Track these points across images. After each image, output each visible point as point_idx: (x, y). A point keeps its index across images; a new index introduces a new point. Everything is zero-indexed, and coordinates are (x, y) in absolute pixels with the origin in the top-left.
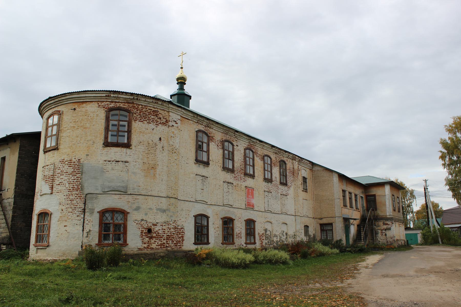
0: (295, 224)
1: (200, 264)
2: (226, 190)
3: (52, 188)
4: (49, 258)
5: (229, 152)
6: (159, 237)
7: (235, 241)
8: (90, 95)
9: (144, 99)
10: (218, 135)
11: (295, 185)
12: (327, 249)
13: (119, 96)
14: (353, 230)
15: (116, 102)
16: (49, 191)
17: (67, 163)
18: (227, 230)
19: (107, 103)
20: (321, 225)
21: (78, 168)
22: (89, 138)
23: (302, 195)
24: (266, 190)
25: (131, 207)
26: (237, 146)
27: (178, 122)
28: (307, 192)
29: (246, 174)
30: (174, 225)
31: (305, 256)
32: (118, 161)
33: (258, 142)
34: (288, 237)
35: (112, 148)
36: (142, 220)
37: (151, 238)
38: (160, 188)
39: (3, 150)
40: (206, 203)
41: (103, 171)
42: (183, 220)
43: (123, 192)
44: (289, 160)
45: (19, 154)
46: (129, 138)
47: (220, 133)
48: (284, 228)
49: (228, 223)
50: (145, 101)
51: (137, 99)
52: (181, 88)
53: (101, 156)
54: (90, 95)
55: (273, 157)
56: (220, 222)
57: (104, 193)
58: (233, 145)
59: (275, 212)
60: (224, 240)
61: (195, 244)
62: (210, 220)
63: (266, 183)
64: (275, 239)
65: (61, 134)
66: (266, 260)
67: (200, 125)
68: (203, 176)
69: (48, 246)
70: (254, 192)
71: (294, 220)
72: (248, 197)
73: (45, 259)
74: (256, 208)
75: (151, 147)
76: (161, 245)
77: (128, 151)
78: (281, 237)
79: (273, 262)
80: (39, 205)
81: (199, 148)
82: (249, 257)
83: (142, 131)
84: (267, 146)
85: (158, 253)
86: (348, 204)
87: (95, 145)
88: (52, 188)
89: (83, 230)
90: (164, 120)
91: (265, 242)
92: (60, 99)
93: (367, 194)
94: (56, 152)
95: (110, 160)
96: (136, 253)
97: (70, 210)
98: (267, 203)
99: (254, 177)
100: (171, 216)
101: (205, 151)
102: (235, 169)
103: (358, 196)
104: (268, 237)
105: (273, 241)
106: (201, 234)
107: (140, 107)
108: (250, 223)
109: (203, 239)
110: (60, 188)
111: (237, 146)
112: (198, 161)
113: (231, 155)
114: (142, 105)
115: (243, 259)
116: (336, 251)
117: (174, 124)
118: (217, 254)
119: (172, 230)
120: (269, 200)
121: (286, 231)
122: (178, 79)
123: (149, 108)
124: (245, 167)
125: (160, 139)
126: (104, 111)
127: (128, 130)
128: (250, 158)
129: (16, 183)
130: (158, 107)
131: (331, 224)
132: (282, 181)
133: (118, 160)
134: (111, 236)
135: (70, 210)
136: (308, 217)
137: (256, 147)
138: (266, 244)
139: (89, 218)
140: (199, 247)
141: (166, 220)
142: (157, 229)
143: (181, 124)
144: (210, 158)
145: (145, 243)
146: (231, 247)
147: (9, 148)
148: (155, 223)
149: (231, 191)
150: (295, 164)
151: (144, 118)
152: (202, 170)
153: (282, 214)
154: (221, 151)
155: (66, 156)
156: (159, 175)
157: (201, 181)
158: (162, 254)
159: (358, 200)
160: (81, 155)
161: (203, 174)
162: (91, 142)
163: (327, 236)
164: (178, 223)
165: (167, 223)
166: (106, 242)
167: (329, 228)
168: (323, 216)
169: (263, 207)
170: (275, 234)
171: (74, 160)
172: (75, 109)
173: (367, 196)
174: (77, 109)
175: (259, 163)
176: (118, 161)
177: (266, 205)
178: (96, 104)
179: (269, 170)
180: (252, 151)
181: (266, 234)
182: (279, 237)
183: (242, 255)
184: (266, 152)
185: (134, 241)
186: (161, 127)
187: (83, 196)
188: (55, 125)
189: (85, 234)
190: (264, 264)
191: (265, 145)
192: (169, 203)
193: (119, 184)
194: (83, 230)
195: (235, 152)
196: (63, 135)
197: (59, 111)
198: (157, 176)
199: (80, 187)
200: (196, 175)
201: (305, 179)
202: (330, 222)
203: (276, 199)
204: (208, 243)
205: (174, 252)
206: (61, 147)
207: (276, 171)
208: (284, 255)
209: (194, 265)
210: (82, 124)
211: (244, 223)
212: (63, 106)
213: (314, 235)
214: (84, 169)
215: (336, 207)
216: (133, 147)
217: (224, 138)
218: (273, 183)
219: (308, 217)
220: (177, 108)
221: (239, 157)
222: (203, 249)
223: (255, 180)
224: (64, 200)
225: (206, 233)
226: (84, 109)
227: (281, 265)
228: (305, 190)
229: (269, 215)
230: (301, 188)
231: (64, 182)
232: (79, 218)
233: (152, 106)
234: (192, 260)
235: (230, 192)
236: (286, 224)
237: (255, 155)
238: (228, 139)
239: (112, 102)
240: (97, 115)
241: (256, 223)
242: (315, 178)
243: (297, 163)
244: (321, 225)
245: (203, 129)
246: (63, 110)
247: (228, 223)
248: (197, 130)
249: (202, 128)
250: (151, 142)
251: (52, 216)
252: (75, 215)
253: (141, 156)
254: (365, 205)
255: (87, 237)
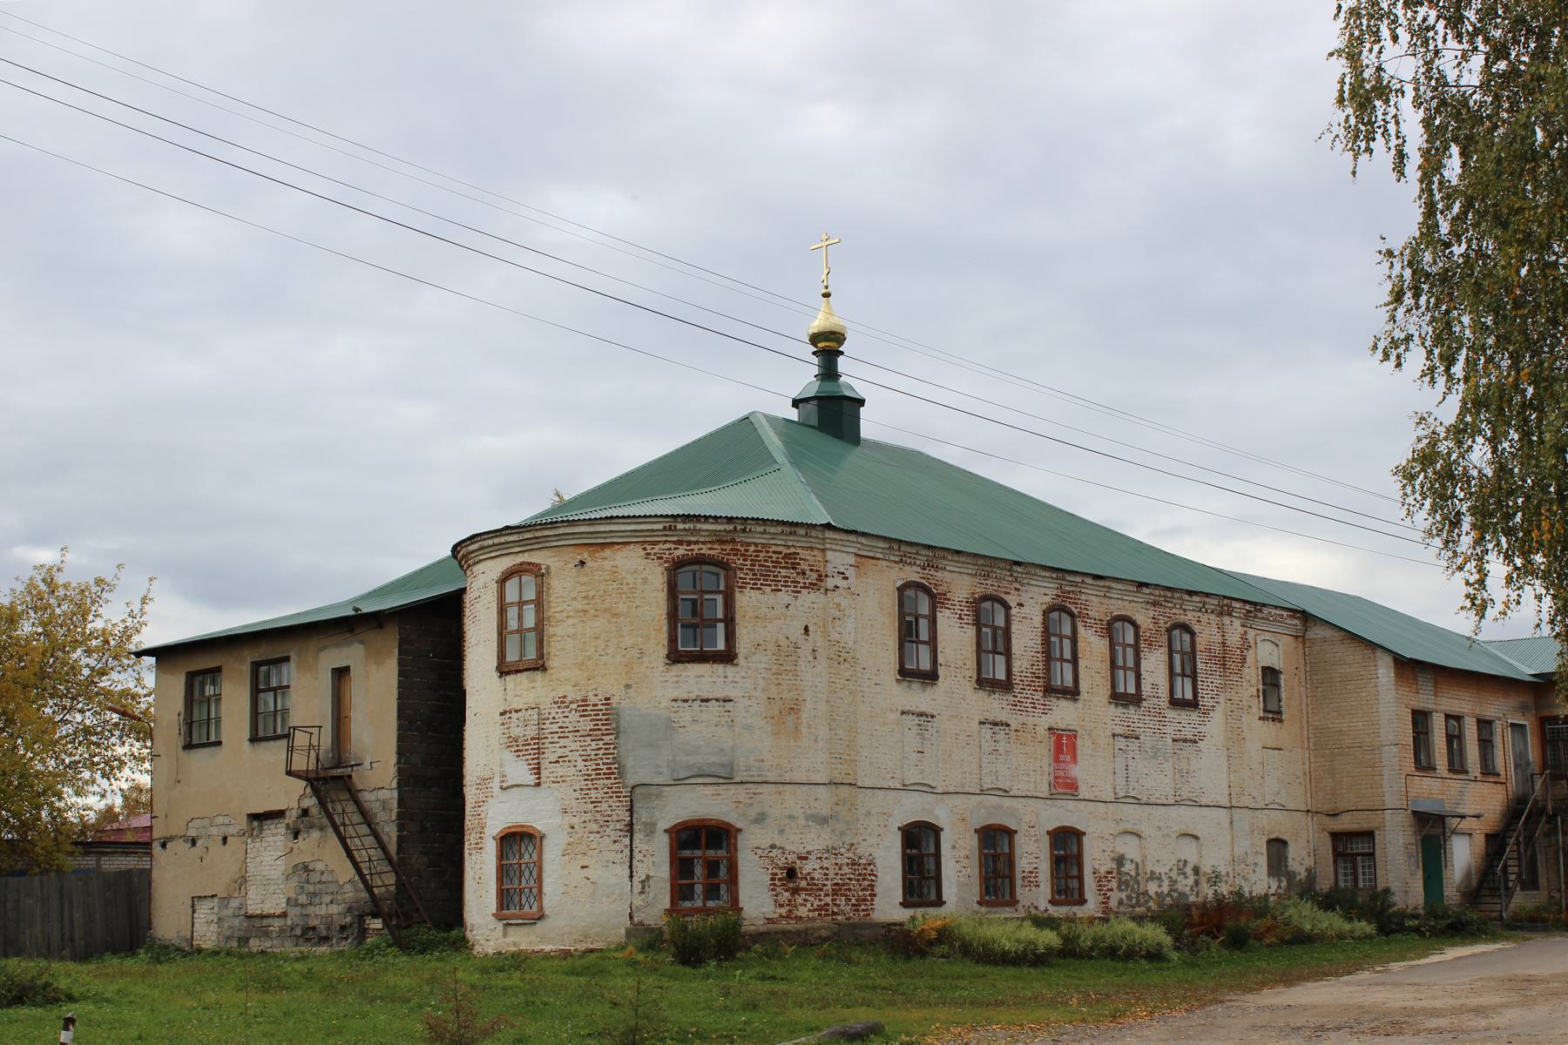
0: (1229, 838)
1: (922, 954)
2: (987, 747)
3: (538, 770)
4: (548, 948)
5: (995, 629)
6: (814, 888)
7: (1019, 897)
8: (623, 528)
9: (761, 529)
10: (960, 585)
11: (1230, 711)
12: (1331, 922)
13: (699, 526)
14: (1462, 855)
15: (689, 543)
16: (532, 779)
17: (574, 706)
18: (995, 862)
19: (668, 546)
20: (1335, 836)
21: (605, 720)
22: (629, 641)
23: (1259, 732)
24: (1119, 730)
25: (744, 815)
26: (1021, 605)
27: (850, 573)
28: (1281, 721)
29: (1049, 690)
30: (851, 855)
31: (1238, 941)
32: (707, 700)
33: (1089, 581)
34: (1203, 880)
35: (689, 666)
36: (773, 846)
37: (796, 891)
38: (813, 761)
39: (336, 645)
40: (930, 789)
41: (670, 726)
42: (871, 840)
43: (724, 777)
44: (1204, 618)
45: (400, 663)
46: (730, 637)
47: (967, 578)
48: (1188, 851)
49: (995, 843)
50: (764, 532)
51: (744, 531)
52: (829, 372)
53: (660, 689)
54: (623, 528)
55: (1143, 618)
56: (974, 841)
57: (678, 782)
58: (1007, 607)
59: (1152, 800)
60: (987, 893)
61: (905, 904)
62: (943, 836)
63: (1120, 709)
64: (1152, 888)
65: (549, 630)
66: (1101, 950)
67: (907, 568)
68: (921, 714)
69: (541, 918)
70: (1079, 742)
71: (1227, 825)
72: (1057, 760)
73: (537, 948)
74: (1084, 792)
75: (786, 655)
76: (820, 908)
77: (730, 670)
78: (1173, 882)
79: (1117, 954)
80: (490, 810)
81: (907, 633)
82: (1049, 938)
83: (762, 614)
84: (1120, 586)
85: (815, 929)
86: (1441, 761)
87: (646, 659)
88: (538, 770)
89: (631, 877)
90: (815, 576)
91: (1115, 897)
92: (538, 534)
93: (1546, 713)
94: (538, 675)
95: (685, 696)
96: (762, 929)
97: (594, 827)
98: (1121, 772)
99: (1078, 693)
100: (842, 833)
101: (924, 643)
102: (1016, 679)
103: (1498, 727)
104: (1127, 883)
105: (1146, 893)
106: (921, 873)
107: (752, 548)
108: (1066, 843)
109: (925, 890)
110: (560, 770)
111: (1021, 605)
112: (906, 674)
113: (1000, 642)
114: (756, 545)
115: (1031, 942)
116: (1364, 927)
117: (838, 581)
118: (964, 930)
119: (846, 869)
120: (1131, 762)
121: (1193, 861)
122: (814, 339)
123: (774, 548)
124: (1048, 669)
125: (806, 629)
126: (661, 569)
127: (726, 615)
128: (1061, 637)
129: (399, 747)
130: (797, 543)
131: (1369, 835)
132: (1178, 695)
133: (705, 696)
134: (699, 889)
135: (594, 827)
136: (1283, 808)
137: (1083, 597)
138: (1121, 902)
139: (644, 847)
140: (919, 911)
141: (830, 844)
142: (808, 867)
143: (858, 575)
144: (941, 659)
145: (781, 906)
146: (1007, 912)
147: (361, 642)
148: (803, 852)
149: (1001, 747)
150: (1228, 629)
151: (765, 578)
152: (918, 697)
153: (1177, 803)
154: (971, 632)
155: (569, 688)
156: (809, 726)
157: (915, 730)
158: (824, 933)
159: (1497, 740)
160: (609, 685)
161: (923, 708)
162: (635, 653)
163: (1355, 875)
164: (860, 851)
165: (832, 851)
166: (687, 904)
167: (1360, 847)
168: (1342, 806)
169: (1108, 787)
170: (1152, 872)
171: (593, 700)
172: (582, 563)
173: (1544, 722)
174: (589, 564)
175: (1093, 646)
176: (707, 700)
177: (1121, 781)
178: (638, 551)
179: (1130, 663)
180: (1071, 615)
181: (1119, 872)
182: (1166, 882)
183: (1029, 932)
184: (1118, 608)
185: (757, 902)
186: (807, 598)
187: (625, 792)
188: (527, 602)
189: (637, 887)
190: (1092, 957)
191: (1113, 585)
192: (834, 799)
193: (713, 759)
194: (631, 877)
195: (1014, 627)
196: (555, 631)
197: (538, 566)
198: (804, 730)
199: (616, 770)
200: (903, 713)
201: (1270, 676)
202: (1366, 826)
203: (1154, 757)
204: (939, 902)
205: (853, 927)
206: (553, 663)
207: (1154, 666)
208: (1155, 934)
209: (908, 958)
210: (606, 605)
211: (1046, 840)
212: (545, 552)
213: (1308, 870)
214: (623, 723)
215: (1385, 772)
216: (741, 660)
217: (980, 590)
218: (1145, 704)
219: (1283, 808)
220: (845, 537)
221: (1026, 639)
222: (928, 919)
223: (1080, 705)
224: (574, 803)
225: (933, 874)
226: (607, 565)
227: (1143, 962)
228: (1273, 714)
229: (1130, 813)
230: (1255, 710)
231: (571, 756)
232: (617, 846)
233: (780, 544)
234: (903, 945)
235: (1001, 750)
236: (1196, 838)
237: (1080, 625)
238: (990, 591)
239: (680, 542)
240: (645, 580)
241: (1085, 840)
242: (1314, 669)
243: (1237, 623)
244: (1335, 836)
245: (915, 578)
246: (548, 562)
247: (995, 843)
248: (899, 583)
249: (912, 574)
250: (783, 642)
251: (545, 842)
252: (607, 841)
253: (761, 683)
254: (1533, 754)
255: (642, 893)
